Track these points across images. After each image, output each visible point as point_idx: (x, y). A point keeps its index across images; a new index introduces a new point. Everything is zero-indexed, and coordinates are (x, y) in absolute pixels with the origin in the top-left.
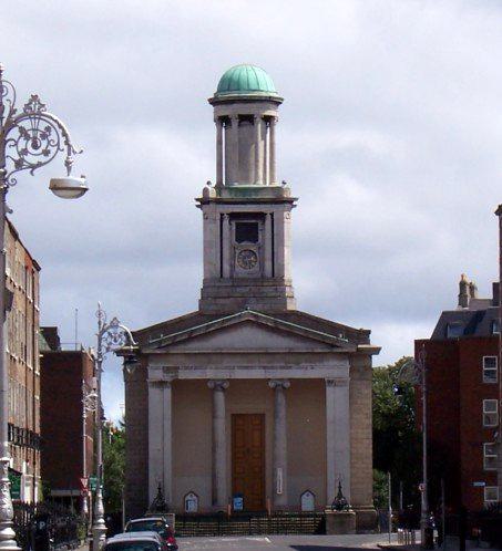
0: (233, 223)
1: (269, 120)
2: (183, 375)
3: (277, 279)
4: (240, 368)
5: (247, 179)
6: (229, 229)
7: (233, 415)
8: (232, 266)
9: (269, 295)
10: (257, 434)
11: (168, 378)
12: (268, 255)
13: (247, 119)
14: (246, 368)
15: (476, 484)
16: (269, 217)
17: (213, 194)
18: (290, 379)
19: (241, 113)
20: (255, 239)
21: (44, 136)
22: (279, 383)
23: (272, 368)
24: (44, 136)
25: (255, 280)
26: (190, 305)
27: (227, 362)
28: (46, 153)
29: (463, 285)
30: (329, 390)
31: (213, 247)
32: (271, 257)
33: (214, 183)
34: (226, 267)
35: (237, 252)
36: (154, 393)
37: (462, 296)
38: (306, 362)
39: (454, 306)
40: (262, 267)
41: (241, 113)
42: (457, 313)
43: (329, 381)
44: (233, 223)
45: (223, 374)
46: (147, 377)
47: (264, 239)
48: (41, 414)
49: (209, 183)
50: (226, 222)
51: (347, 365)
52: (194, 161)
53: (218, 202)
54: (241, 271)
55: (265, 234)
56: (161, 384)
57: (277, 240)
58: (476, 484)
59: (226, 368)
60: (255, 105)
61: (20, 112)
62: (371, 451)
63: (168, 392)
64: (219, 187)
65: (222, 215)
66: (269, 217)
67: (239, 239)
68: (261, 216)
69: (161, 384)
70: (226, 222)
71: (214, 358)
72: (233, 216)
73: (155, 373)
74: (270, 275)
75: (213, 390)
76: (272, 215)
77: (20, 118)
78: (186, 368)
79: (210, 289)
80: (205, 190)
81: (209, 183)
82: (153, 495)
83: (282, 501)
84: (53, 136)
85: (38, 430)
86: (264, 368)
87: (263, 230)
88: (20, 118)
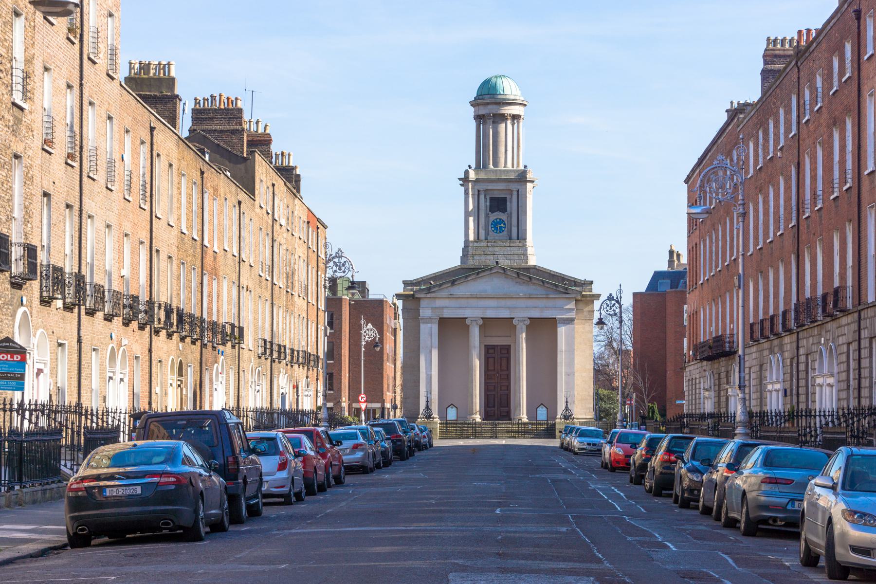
10: (491, 368)
15: (678, 402)
16: (515, 193)
20: (504, 210)
21: (343, 265)
24: (343, 265)
26: (453, 260)
28: (344, 272)
29: (671, 253)
37: (671, 262)
39: (664, 267)
42: (668, 272)
48: (403, 373)
49: (470, 167)
50: (482, 197)
55: (512, 206)
58: (678, 402)
61: (334, 255)
63: (435, 327)
67: (492, 210)
70: (482, 197)
72: (486, 191)
73: (425, 312)
77: (333, 258)
80: (467, 172)
84: (347, 265)
85: (629, 345)
88: (333, 258)
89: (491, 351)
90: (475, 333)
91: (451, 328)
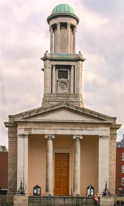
0: (57, 70)
1: (73, 27)
2: (33, 132)
3: (77, 95)
4: (60, 129)
5: (65, 52)
6: (55, 73)
7: (55, 153)
8: (57, 89)
9: (73, 101)
11: (27, 133)
12: (67, 12)
13: (64, 25)
14: (63, 129)
16: (73, 67)
17: (48, 56)
18: (83, 135)
19: (61, 22)
22: (78, 137)
23: (75, 130)
25: (66, 94)
26: (39, 105)
27: (54, 126)
30: (101, 141)
31: (49, 82)
32: (73, 85)
33: (49, 52)
34: (54, 89)
35: (59, 83)
36: (20, 140)
38: (90, 127)
40: (69, 90)
41: (61, 22)
43: (100, 137)
44: (57, 70)
45: (52, 132)
46: (17, 132)
47: (70, 79)
48: (56, 171)
50: (54, 69)
51: (109, 128)
52: (42, 42)
53: (51, 60)
54: (60, 91)
56: (23, 136)
57: (76, 78)
59: (54, 129)
60: (68, 19)
62: (115, 170)
63: (26, 140)
64: (51, 54)
65: (52, 66)
66: (73, 67)
67: (59, 77)
68: (69, 67)
69: (23, 136)
70: (54, 69)
71: (47, 124)
72: (57, 67)
73: (21, 131)
74: (73, 93)
75: (47, 139)
76: (74, 66)
78: (35, 129)
79: (47, 98)
81: (47, 52)
82: (19, 186)
83: (78, 192)
86: (71, 129)
87: (70, 74)
89: (58, 157)
90: (50, 143)
91: (36, 142)
